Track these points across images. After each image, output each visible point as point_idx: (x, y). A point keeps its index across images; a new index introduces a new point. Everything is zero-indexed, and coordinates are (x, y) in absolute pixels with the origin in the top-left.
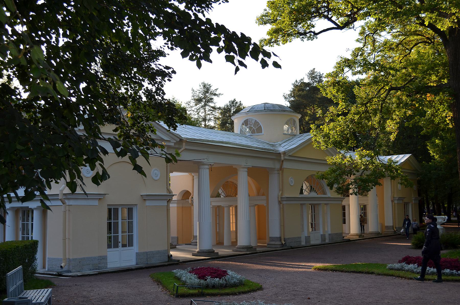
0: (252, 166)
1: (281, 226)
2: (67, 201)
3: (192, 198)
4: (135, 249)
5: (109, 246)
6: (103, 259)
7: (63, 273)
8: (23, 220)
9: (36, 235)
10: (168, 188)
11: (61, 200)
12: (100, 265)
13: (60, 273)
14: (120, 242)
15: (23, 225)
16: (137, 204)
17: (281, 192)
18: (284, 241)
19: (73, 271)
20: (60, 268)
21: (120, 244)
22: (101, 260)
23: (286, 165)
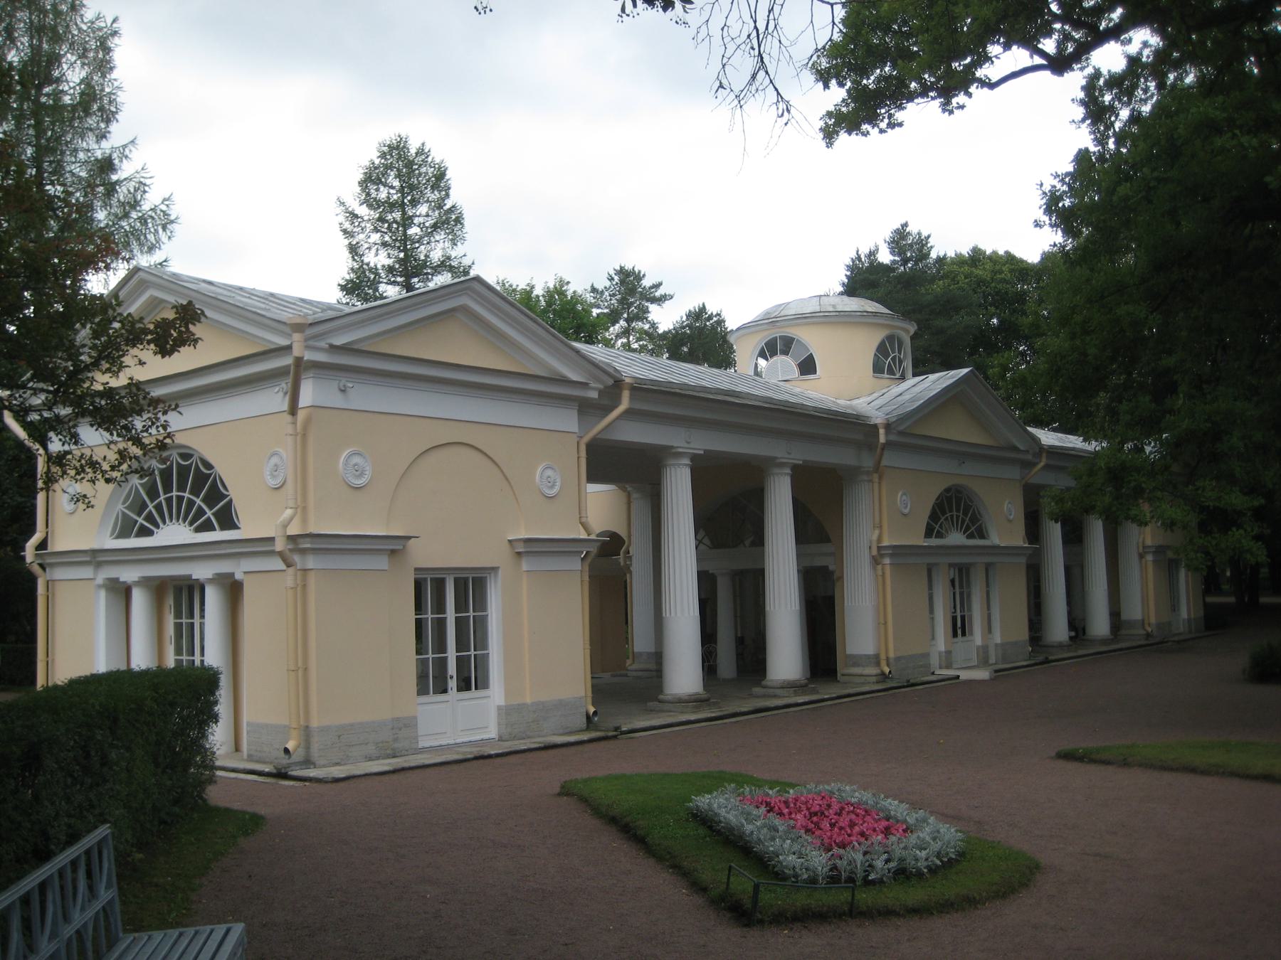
0: (705, 451)
1: (879, 624)
2: (297, 558)
3: (628, 553)
4: (496, 694)
5: (423, 690)
6: (406, 726)
7: (292, 771)
8: (178, 615)
9: (213, 655)
10: (641, 508)
11: (280, 554)
12: (396, 745)
13: (283, 771)
14: (452, 677)
15: (178, 627)
16: (498, 568)
17: (877, 532)
18: (888, 665)
19: (322, 762)
20: (283, 752)
21: (452, 684)
22: (400, 729)
23: (889, 460)
